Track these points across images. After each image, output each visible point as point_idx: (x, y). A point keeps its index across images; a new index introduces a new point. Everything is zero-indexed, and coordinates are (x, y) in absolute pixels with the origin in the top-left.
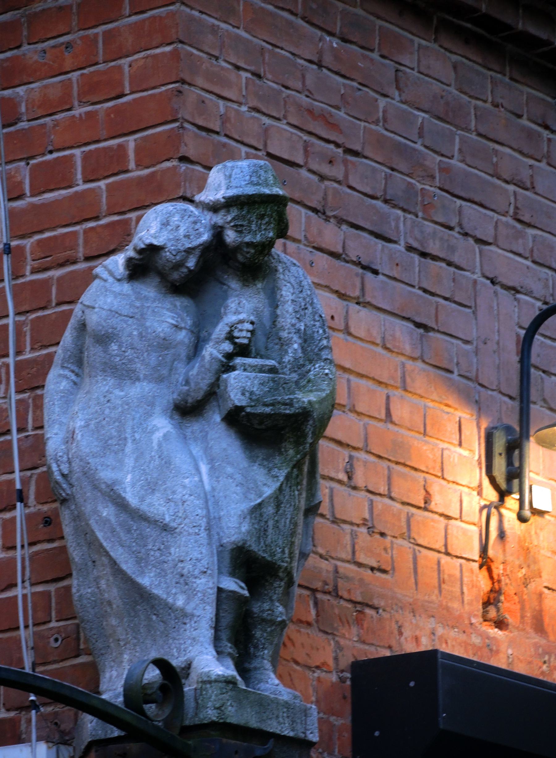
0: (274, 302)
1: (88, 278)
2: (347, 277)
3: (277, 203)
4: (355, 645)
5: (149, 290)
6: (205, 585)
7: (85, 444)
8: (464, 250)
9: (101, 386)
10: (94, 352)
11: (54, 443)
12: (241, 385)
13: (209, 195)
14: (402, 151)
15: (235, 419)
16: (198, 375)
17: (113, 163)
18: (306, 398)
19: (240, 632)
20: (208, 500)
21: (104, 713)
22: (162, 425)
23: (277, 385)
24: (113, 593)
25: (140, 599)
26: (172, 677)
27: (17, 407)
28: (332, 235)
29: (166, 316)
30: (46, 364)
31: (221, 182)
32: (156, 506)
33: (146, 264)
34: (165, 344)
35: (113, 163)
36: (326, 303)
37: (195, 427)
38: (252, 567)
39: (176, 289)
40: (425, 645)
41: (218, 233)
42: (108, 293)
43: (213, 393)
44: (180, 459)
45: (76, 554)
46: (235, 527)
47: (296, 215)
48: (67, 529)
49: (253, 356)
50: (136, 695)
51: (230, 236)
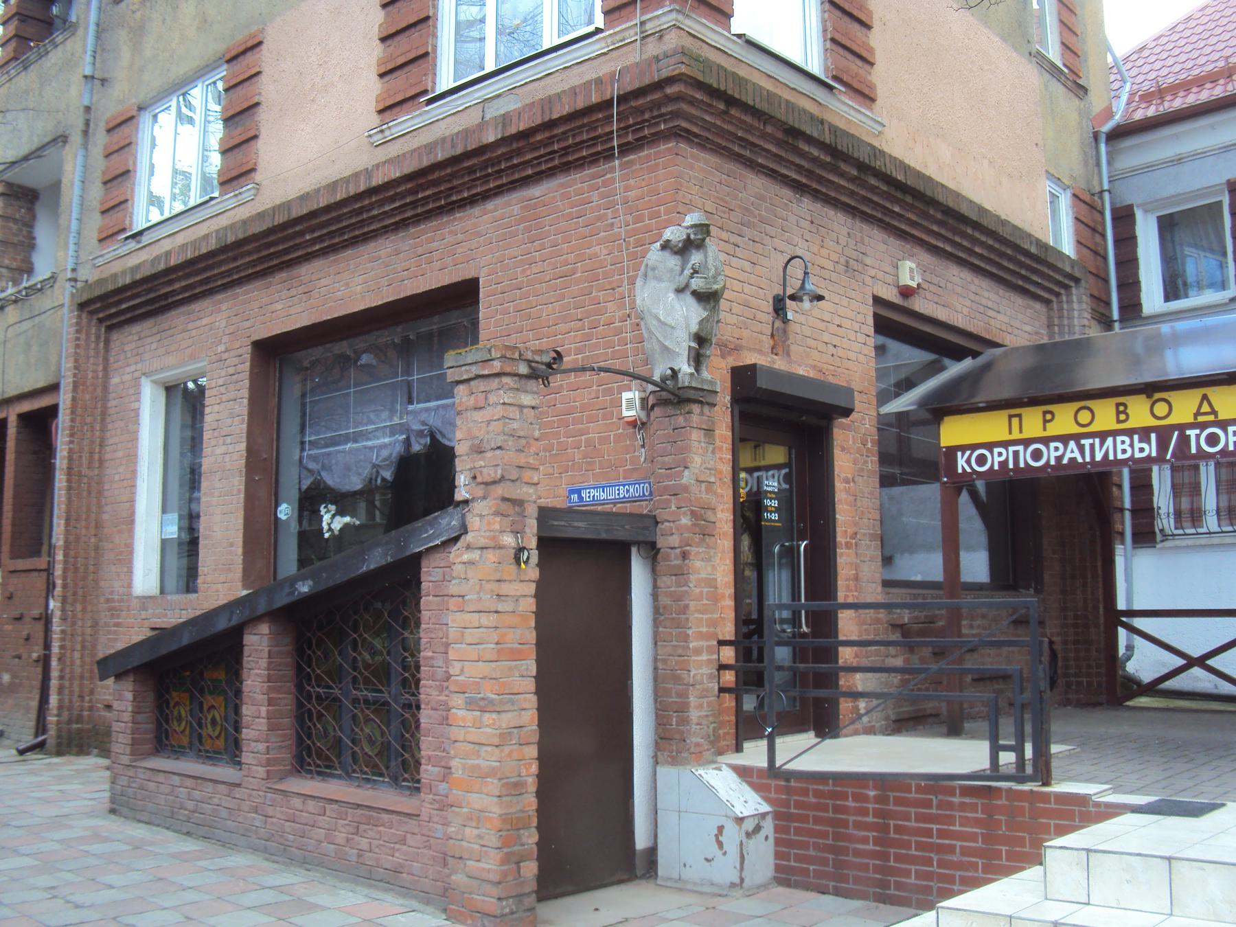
0: (706, 257)
1: (649, 250)
2: (730, 248)
3: (707, 226)
4: (732, 361)
5: (667, 254)
6: (685, 345)
7: (647, 302)
8: (767, 240)
9: (652, 283)
10: (650, 273)
11: (638, 302)
12: (696, 284)
13: (685, 224)
14: (746, 209)
15: (694, 293)
16: (682, 280)
17: (657, 215)
18: (715, 287)
19: (697, 359)
20: (686, 319)
21: (654, 383)
22: (672, 296)
23: (707, 283)
24: (657, 347)
25: (665, 349)
26: (675, 373)
27: (1131, 792)
28: (725, 235)
29: (673, 261)
30: (635, 277)
31: (690, 219)
32: (670, 321)
33: (666, 246)
34: (672, 270)
35: (657, 215)
36: (722, 257)
37: (681, 296)
38: (701, 339)
39: (676, 253)
40: (753, 361)
41: (688, 236)
42: (655, 255)
43: (687, 286)
44: (677, 306)
45: (646, 335)
46: (694, 328)
47: (713, 229)
48: (643, 327)
49: (639, 873)
50: (664, 379)
51: (692, 237)
